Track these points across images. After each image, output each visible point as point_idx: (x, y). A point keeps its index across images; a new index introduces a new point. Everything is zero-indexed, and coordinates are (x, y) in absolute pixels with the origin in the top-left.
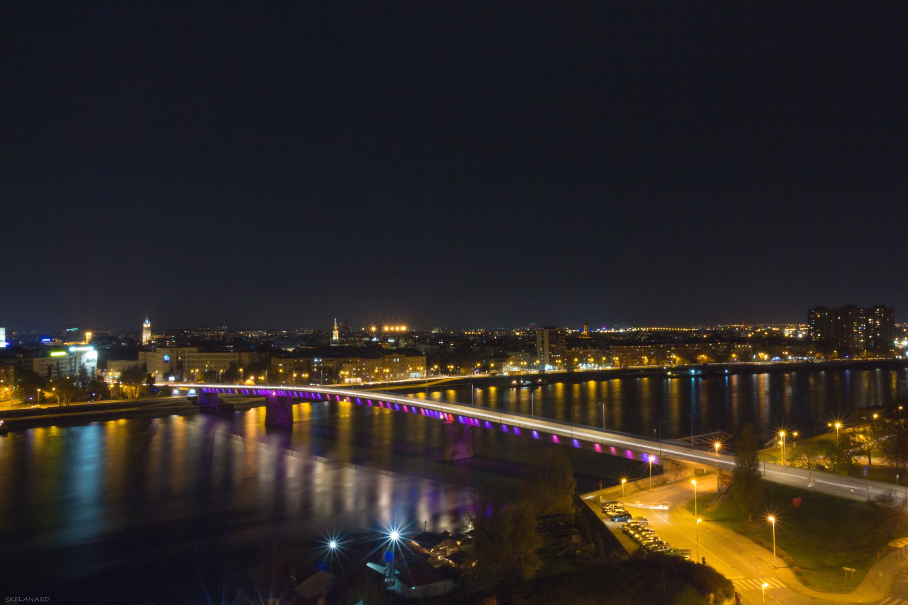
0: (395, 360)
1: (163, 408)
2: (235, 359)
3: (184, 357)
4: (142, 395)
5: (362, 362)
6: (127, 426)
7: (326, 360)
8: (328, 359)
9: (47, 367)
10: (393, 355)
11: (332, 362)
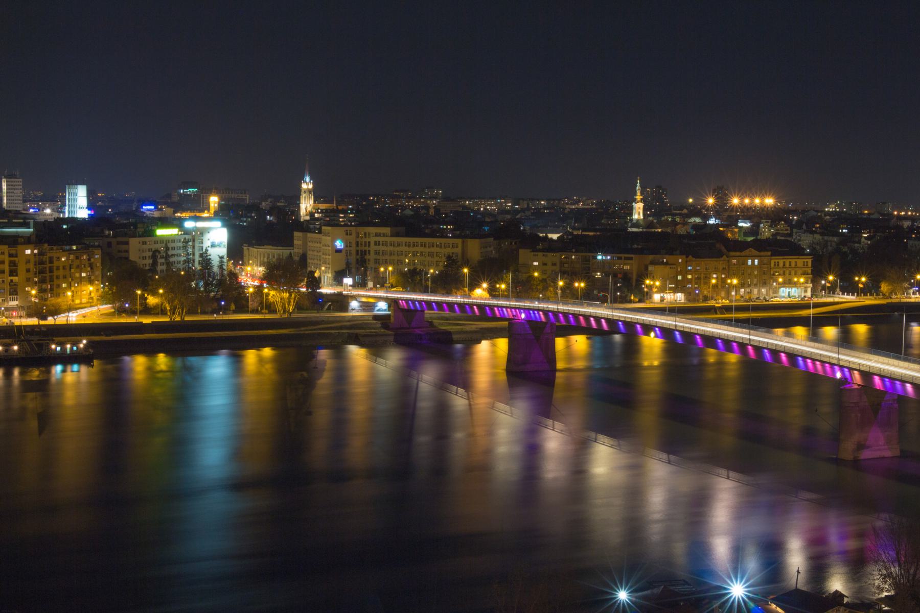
0: (750, 262)
1: (333, 332)
2: (455, 250)
3: (369, 242)
4: (299, 307)
5: (687, 263)
6: (276, 360)
7: (620, 258)
8: (623, 256)
9: (151, 254)
10: (747, 252)
11: (630, 261)
